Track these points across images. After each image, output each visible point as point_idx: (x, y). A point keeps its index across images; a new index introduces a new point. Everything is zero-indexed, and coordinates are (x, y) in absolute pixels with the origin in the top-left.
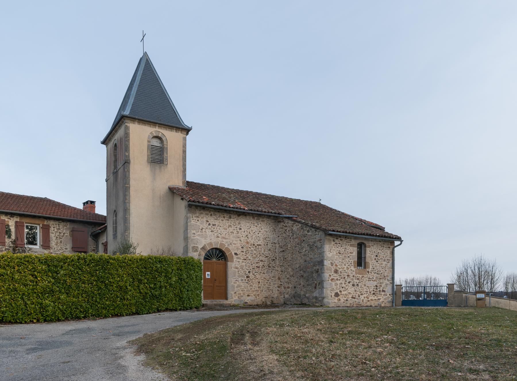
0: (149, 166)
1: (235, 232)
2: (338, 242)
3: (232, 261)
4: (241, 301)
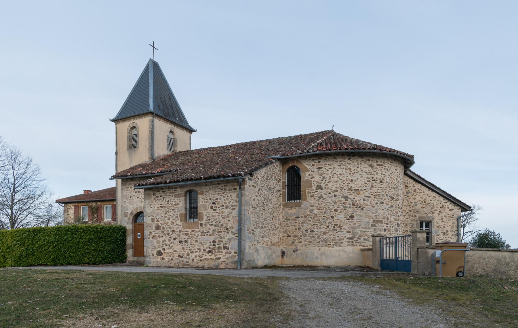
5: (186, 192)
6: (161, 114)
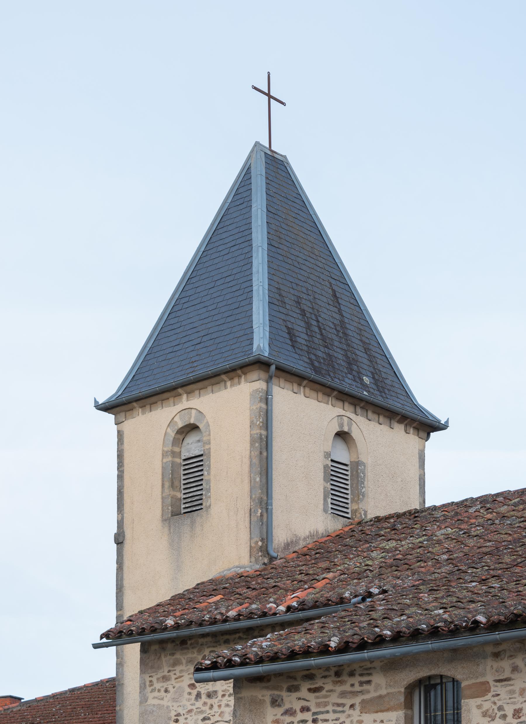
0: (166, 530)
2: (297, 706)
5: (410, 689)
6: (300, 365)
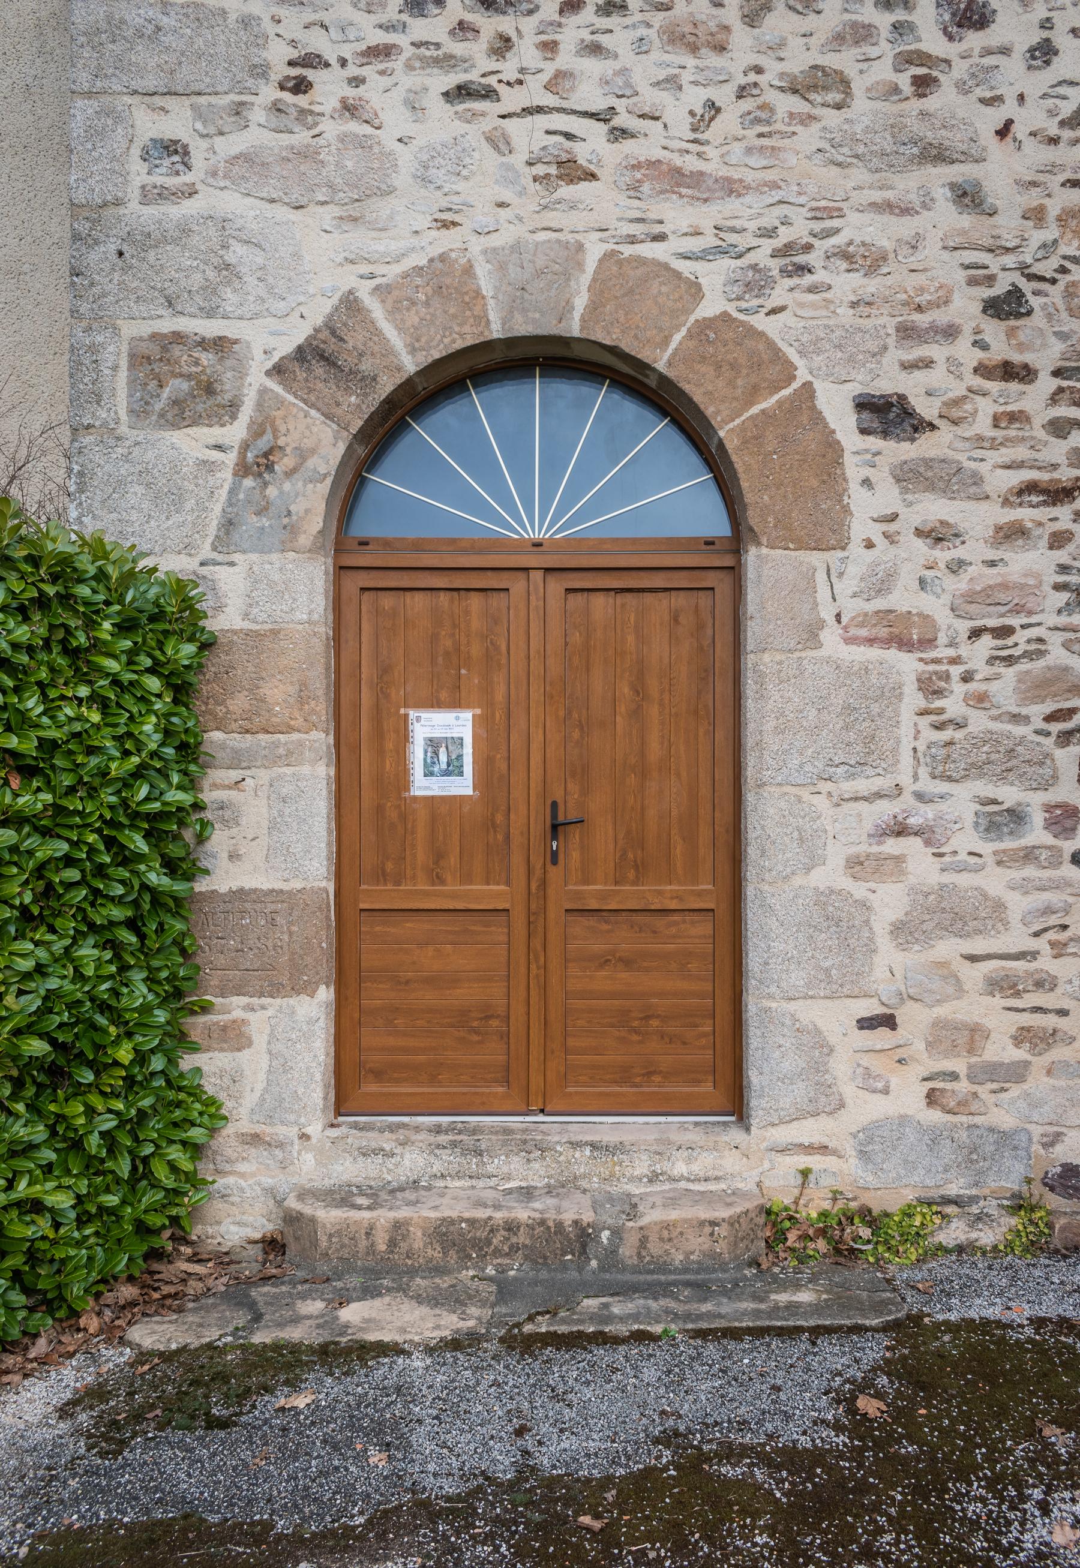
1: (875, 69)
3: (827, 533)
4: (982, 1149)
